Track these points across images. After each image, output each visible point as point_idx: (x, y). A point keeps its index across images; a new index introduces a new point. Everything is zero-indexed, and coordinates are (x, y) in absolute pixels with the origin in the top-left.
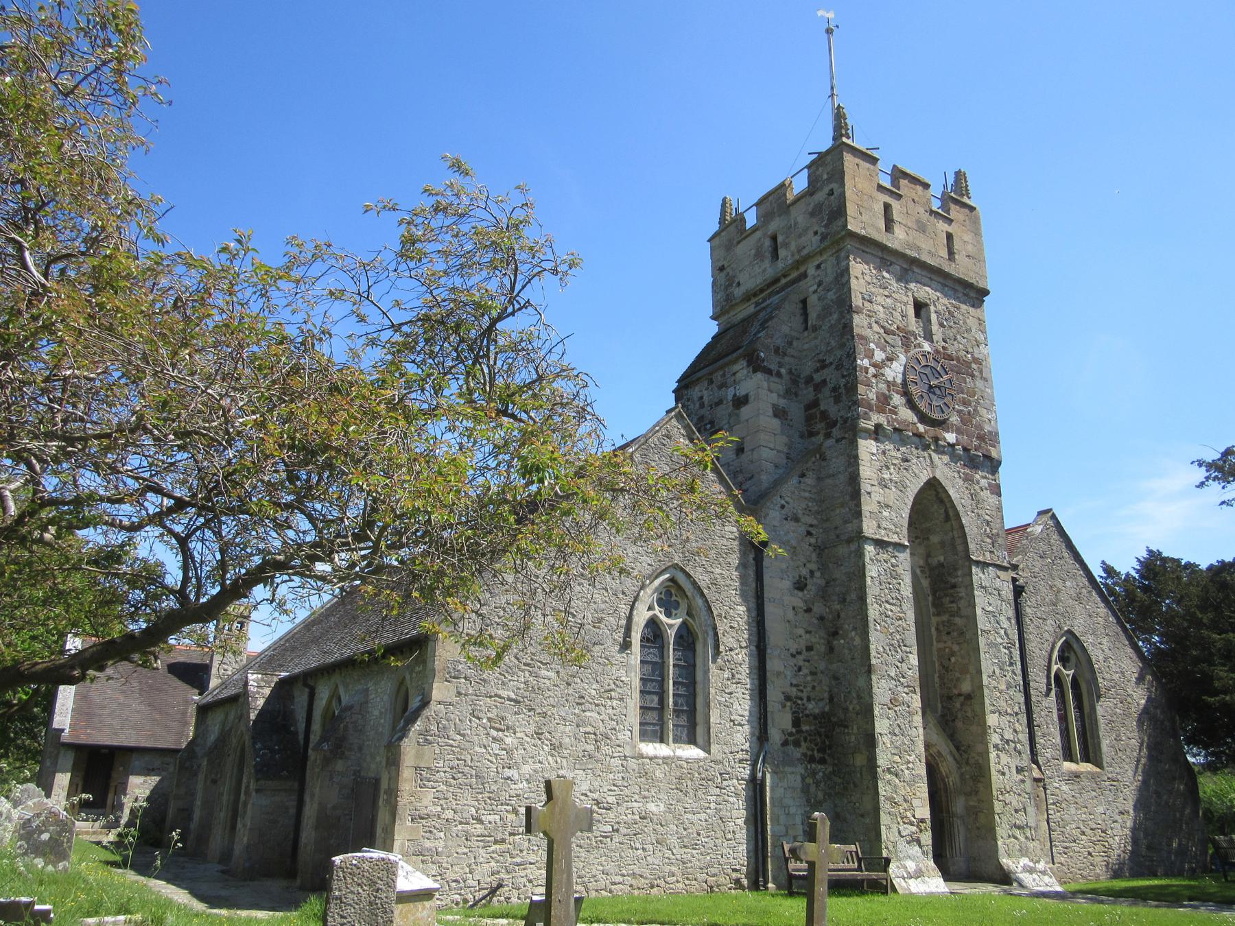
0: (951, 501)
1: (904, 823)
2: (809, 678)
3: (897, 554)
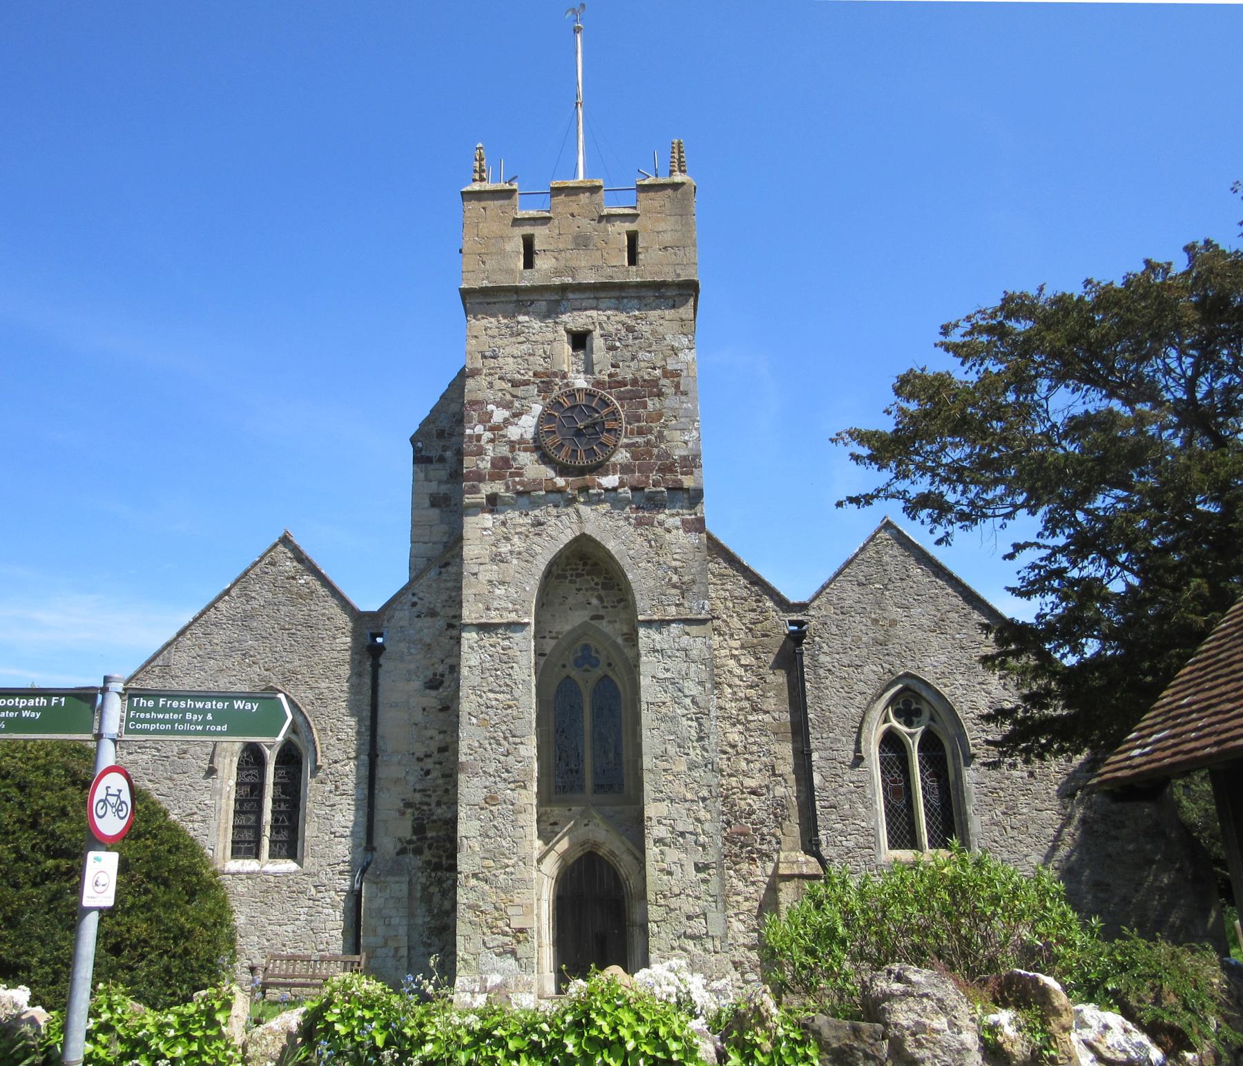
1: (493, 933)
2: (440, 781)
3: (511, 635)
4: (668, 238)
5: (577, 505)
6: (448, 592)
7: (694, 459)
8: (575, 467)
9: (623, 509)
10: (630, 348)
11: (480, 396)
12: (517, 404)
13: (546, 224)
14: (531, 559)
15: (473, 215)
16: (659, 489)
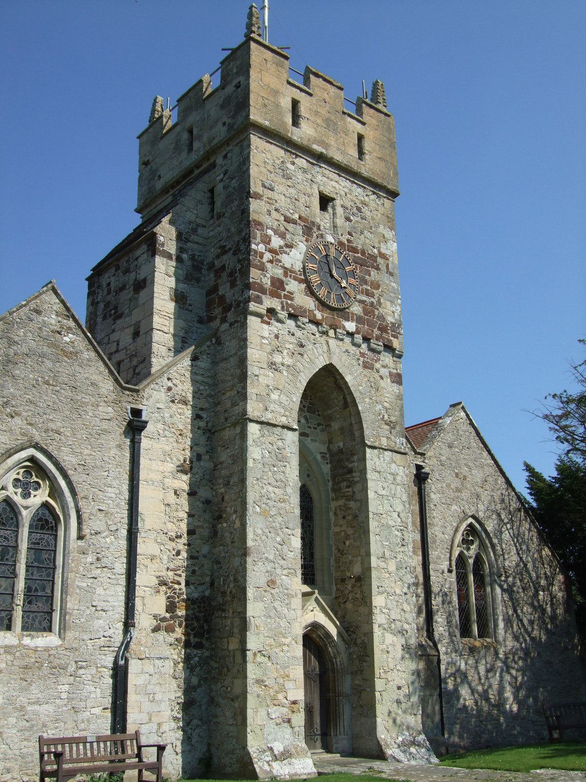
0: (348, 388)
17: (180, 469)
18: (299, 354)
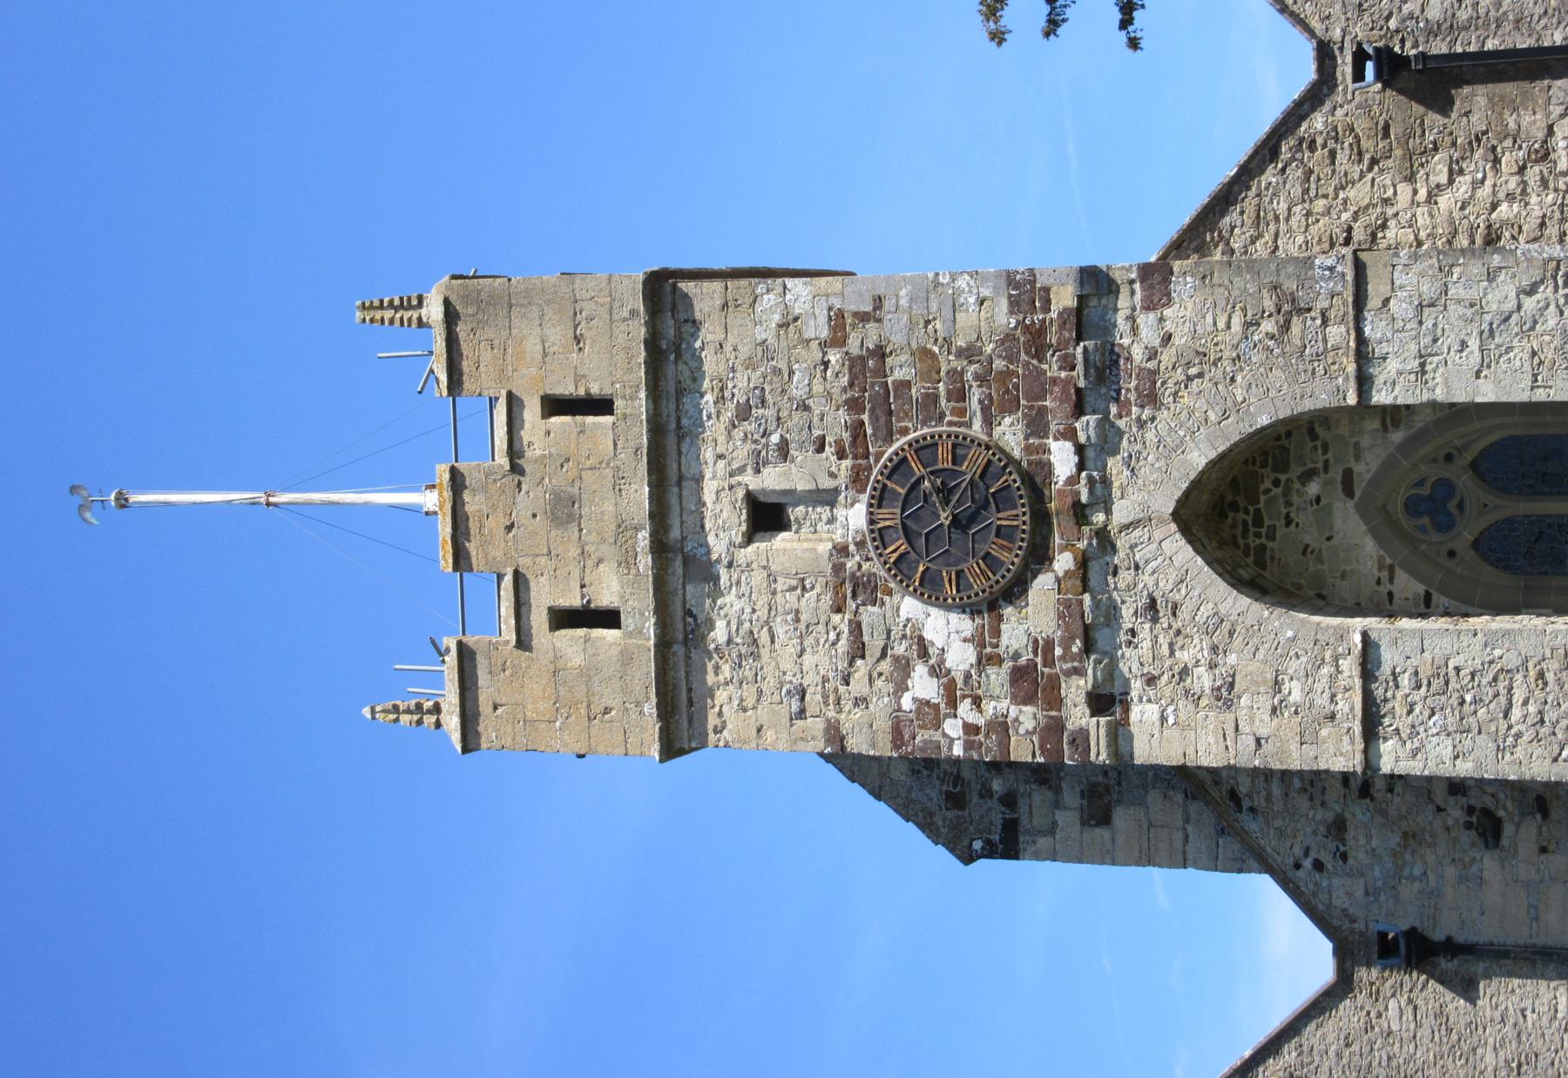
4: (558, 335)
5: (1113, 528)
6: (1293, 794)
7: (1017, 286)
8: (1033, 532)
9: (1120, 433)
10: (784, 414)
11: (883, 724)
12: (900, 649)
13: (527, 581)
14: (1226, 626)
15: (509, 729)
16: (1080, 358)
17: (1490, 840)
18: (1174, 614)
